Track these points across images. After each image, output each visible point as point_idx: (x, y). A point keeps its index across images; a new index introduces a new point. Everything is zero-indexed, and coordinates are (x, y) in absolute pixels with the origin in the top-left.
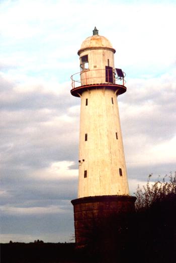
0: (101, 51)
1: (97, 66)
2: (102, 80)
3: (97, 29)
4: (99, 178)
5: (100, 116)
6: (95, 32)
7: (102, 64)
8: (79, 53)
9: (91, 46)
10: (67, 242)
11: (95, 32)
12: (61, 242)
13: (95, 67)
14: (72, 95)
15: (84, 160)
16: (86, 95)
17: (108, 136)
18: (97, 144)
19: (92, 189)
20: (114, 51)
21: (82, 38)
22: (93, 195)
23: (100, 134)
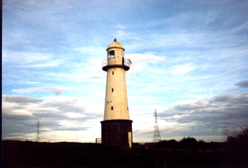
0: (121, 50)
1: (119, 57)
2: (121, 63)
3: (116, 39)
4: (119, 111)
5: (120, 80)
6: (115, 40)
7: (121, 56)
8: (107, 50)
9: (116, 46)
10: (86, 142)
11: (115, 40)
12: (92, 142)
13: (118, 57)
14: (103, 71)
15: (111, 101)
16: (112, 70)
17: (123, 91)
18: (235, 61)
19: (116, 115)
20: (124, 50)
21: (114, 39)
22: (116, 119)
23: (120, 89)
